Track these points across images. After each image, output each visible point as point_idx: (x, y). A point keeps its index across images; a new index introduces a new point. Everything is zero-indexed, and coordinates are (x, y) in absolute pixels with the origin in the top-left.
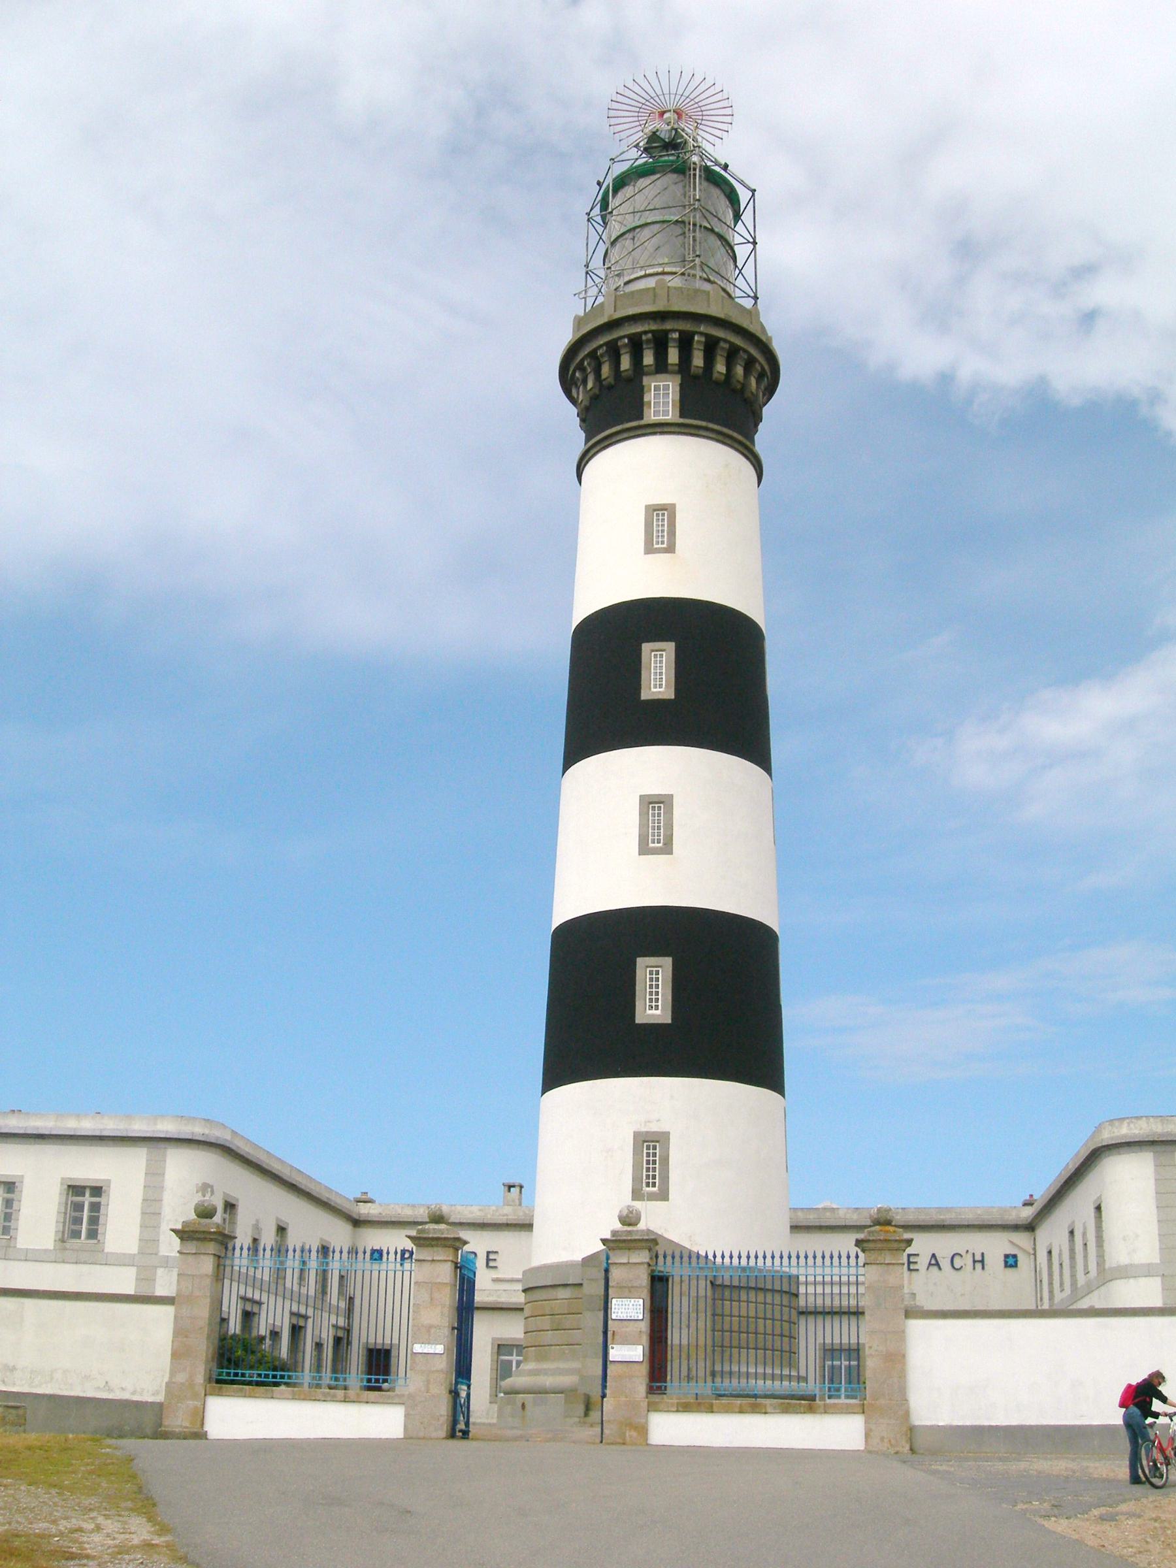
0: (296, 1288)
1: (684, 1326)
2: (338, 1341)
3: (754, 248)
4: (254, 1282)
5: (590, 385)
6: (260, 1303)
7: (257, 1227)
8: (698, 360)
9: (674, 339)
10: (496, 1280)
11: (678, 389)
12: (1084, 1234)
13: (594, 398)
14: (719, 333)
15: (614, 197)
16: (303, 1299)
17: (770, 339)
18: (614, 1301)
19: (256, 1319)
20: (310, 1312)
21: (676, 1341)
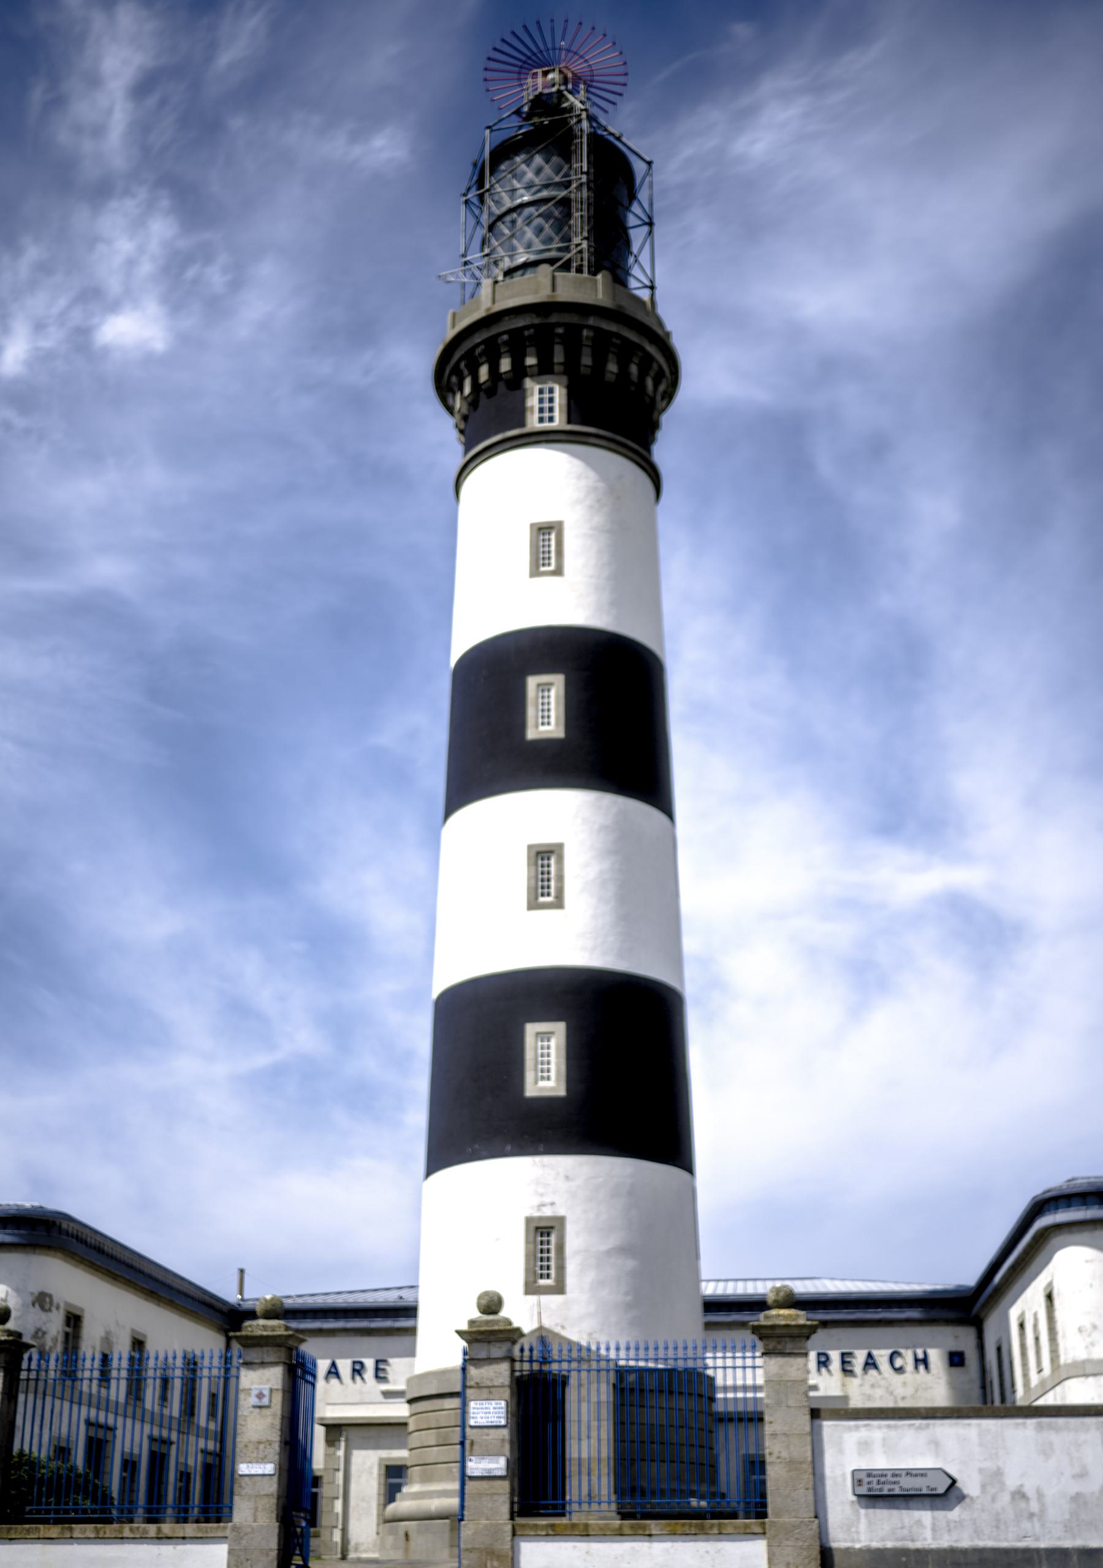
0: (157, 1409)
1: (584, 1436)
2: (207, 1468)
3: (650, 232)
4: (105, 1405)
5: (467, 390)
6: (113, 1429)
7: (107, 1340)
8: (586, 360)
9: (559, 335)
10: (387, 1394)
11: (564, 391)
12: (1035, 1326)
13: (473, 403)
14: (605, 325)
15: (491, 174)
16: (166, 1423)
17: (668, 334)
18: (472, 1404)
19: (110, 1445)
20: (174, 1436)
21: (575, 1455)
